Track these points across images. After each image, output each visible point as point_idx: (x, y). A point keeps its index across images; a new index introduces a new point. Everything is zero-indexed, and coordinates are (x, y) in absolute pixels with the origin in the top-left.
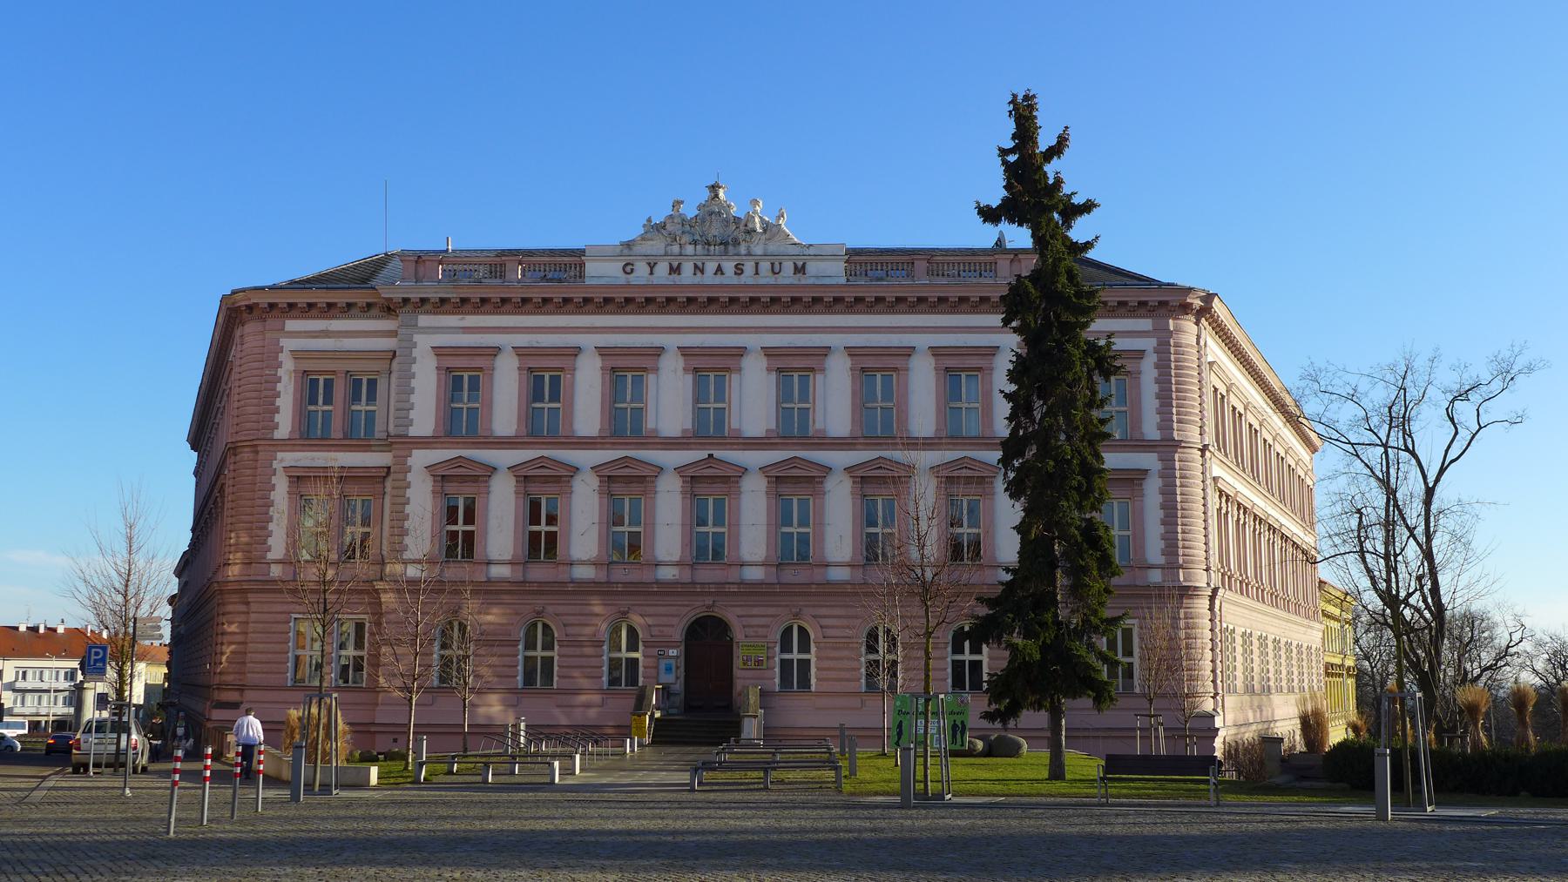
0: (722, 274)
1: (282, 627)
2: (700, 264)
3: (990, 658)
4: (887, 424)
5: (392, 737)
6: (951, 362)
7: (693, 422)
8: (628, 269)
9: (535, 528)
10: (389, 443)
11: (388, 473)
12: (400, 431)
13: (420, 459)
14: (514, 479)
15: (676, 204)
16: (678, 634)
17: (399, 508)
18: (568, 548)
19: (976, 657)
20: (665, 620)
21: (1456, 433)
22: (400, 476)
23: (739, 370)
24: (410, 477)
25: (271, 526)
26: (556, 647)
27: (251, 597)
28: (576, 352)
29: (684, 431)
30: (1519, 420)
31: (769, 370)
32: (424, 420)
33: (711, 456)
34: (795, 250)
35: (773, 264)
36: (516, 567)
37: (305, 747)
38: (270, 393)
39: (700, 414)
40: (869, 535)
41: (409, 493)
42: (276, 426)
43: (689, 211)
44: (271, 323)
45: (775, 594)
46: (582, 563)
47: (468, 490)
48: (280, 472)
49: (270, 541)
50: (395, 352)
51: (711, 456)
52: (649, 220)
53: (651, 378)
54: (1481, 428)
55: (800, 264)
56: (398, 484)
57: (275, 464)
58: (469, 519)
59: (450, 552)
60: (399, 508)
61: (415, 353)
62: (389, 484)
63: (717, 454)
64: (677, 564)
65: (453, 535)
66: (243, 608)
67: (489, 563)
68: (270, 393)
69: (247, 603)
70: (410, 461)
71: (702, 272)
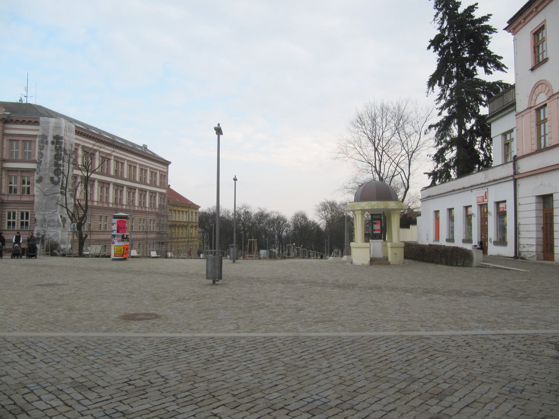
3: (31, 220)
19: (14, 220)
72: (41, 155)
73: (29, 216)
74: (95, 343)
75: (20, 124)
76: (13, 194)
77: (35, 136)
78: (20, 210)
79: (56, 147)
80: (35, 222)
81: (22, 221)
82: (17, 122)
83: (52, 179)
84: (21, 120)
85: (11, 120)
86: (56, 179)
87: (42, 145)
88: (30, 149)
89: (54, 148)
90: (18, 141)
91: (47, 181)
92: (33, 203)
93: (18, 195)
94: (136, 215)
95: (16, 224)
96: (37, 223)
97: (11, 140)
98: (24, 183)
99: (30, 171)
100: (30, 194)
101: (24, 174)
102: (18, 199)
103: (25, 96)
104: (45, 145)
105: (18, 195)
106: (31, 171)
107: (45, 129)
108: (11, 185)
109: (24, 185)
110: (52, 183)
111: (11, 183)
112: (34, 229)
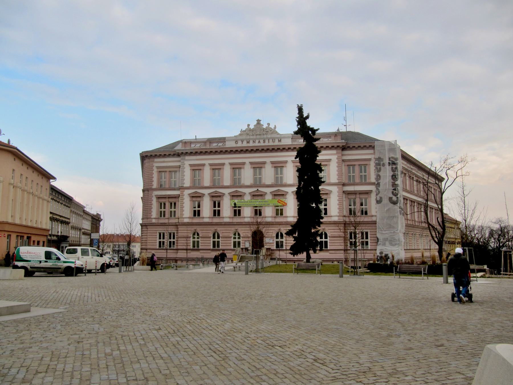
0: (260, 143)
1: (155, 234)
2: (254, 141)
3: (371, 240)
4: (199, 183)
5: (294, 262)
6: (214, 167)
7: (274, 180)
8: (236, 143)
9: (215, 209)
10: (179, 189)
11: (179, 196)
12: (182, 185)
13: (187, 192)
14: (230, 196)
15: (249, 125)
16: (250, 235)
17: (182, 204)
18: (223, 214)
19: (326, 240)
20: (246, 231)
21: (448, 179)
22: (182, 196)
23: (265, 167)
24: (184, 197)
25: (152, 210)
26: (241, 238)
27: (148, 227)
28: (286, 162)
29: (251, 183)
30: (468, 174)
31: (272, 167)
32: (187, 183)
33: (258, 190)
34: (278, 136)
35: (273, 140)
36: (156, 219)
37: (286, 265)
38: (151, 177)
39: (255, 179)
40: (350, 208)
41: (184, 201)
42: (153, 185)
43: (252, 127)
44: (151, 160)
45: (274, 224)
46: (226, 217)
47: (218, 199)
48: (154, 196)
49: (152, 213)
50: (180, 166)
51: (258, 190)
52: (242, 130)
53: (263, 170)
54: (457, 177)
55: (280, 140)
56: (182, 198)
57: (153, 194)
58: (219, 206)
59: (215, 214)
60: (182, 204)
61: (185, 166)
62: (180, 198)
63: (260, 189)
64: (250, 217)
65: (161, 212)
66: (146, 229)
67: (203, 218)
68: (151, 177)
69: (147, 228)
70: (184, 193)
71: (255, 142)
72: (378, 177)
73: (175, 236)
74: (234, 347)
75: (162, 158)
76: (279, 216)
77: (370, 160)
78: (158, 231)
79: (392, 168)
80: (378, 241)
81: (214, 240)
82: (354, 148)
83: (390, 199)
84: (357, 146)
85: (349, 147)
86: (394, 198)
87: (379, 167)
88: (365, 172)
89: (390, 169)
90: (355, 165)
91: (386, 201)
92: (376, 223)
93: (166, 218)
94: (270, 229)
95: (284, 244)
96: (379, 243)
97: (348, 165)
98: (362, 205)
99: (368, 193)
100: (166, 217)
101: (362, 196)
102: (166, 221)
103: (345, 126)
104: (382, 167)
105: (166, 218)
106: (368, 193)
107: (380, 152)
108: (350, 207)
109: (362, 207)
110: (391, 203)
111: (350, 205)
112: (376, 247)
